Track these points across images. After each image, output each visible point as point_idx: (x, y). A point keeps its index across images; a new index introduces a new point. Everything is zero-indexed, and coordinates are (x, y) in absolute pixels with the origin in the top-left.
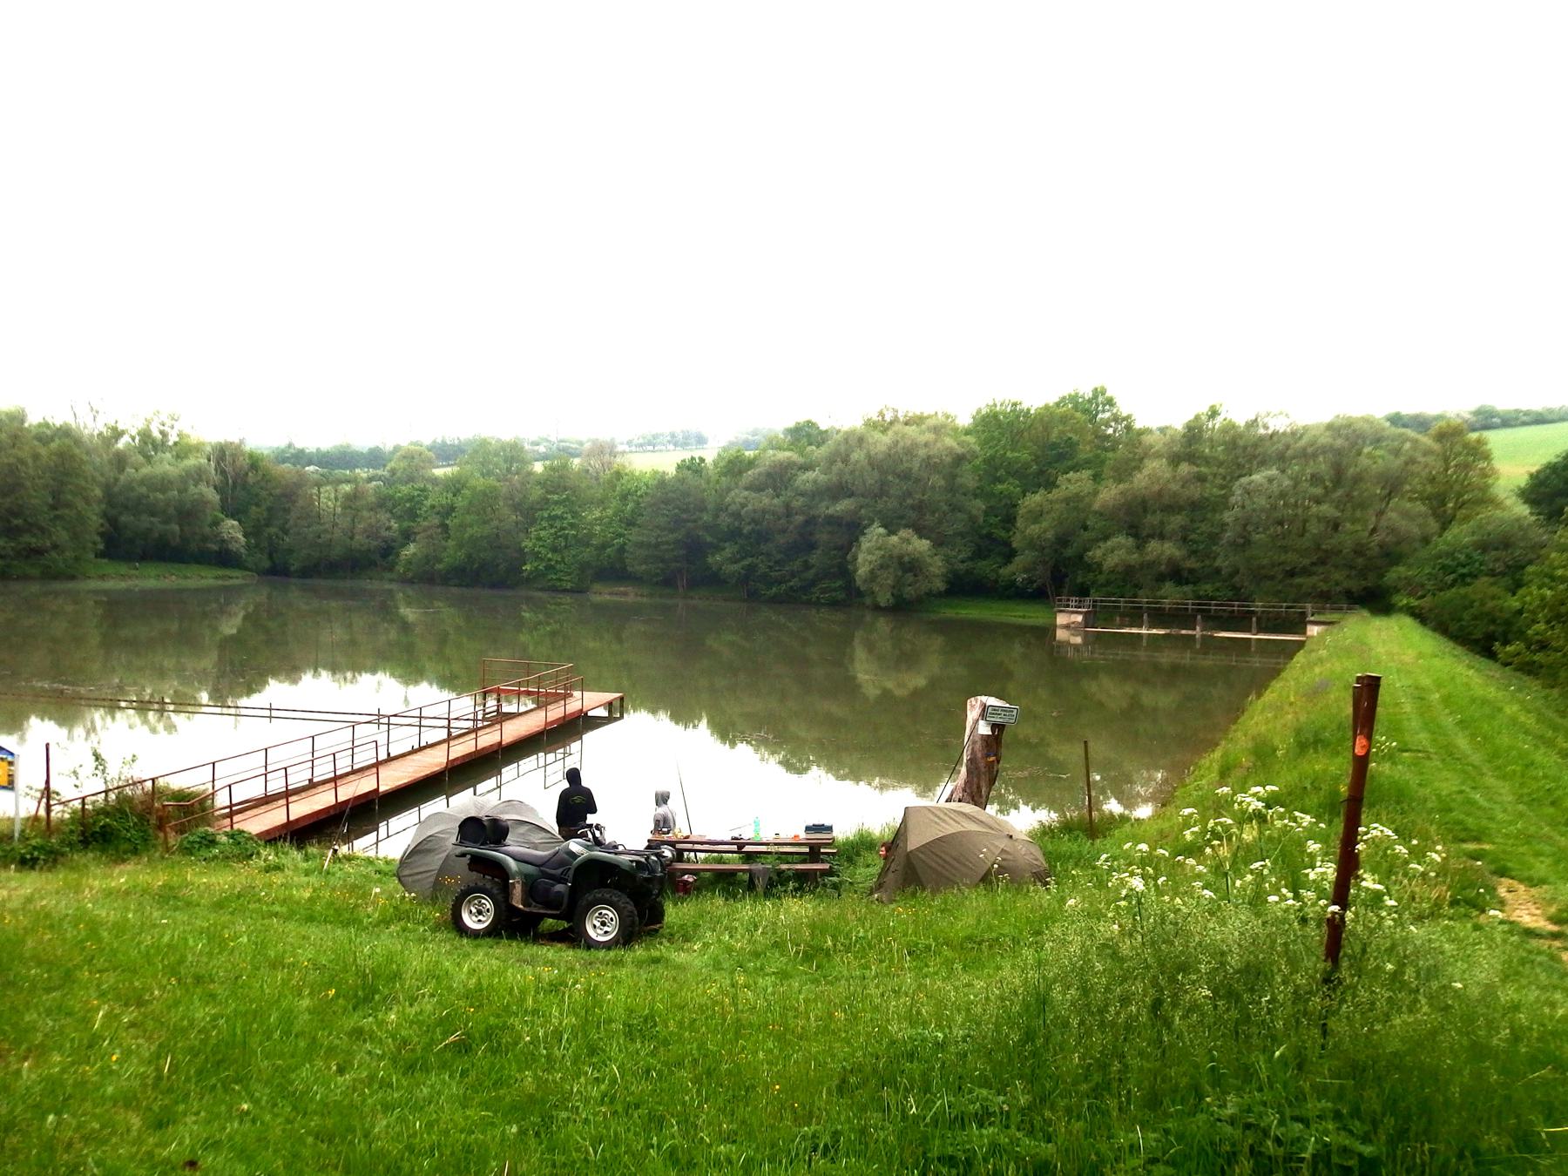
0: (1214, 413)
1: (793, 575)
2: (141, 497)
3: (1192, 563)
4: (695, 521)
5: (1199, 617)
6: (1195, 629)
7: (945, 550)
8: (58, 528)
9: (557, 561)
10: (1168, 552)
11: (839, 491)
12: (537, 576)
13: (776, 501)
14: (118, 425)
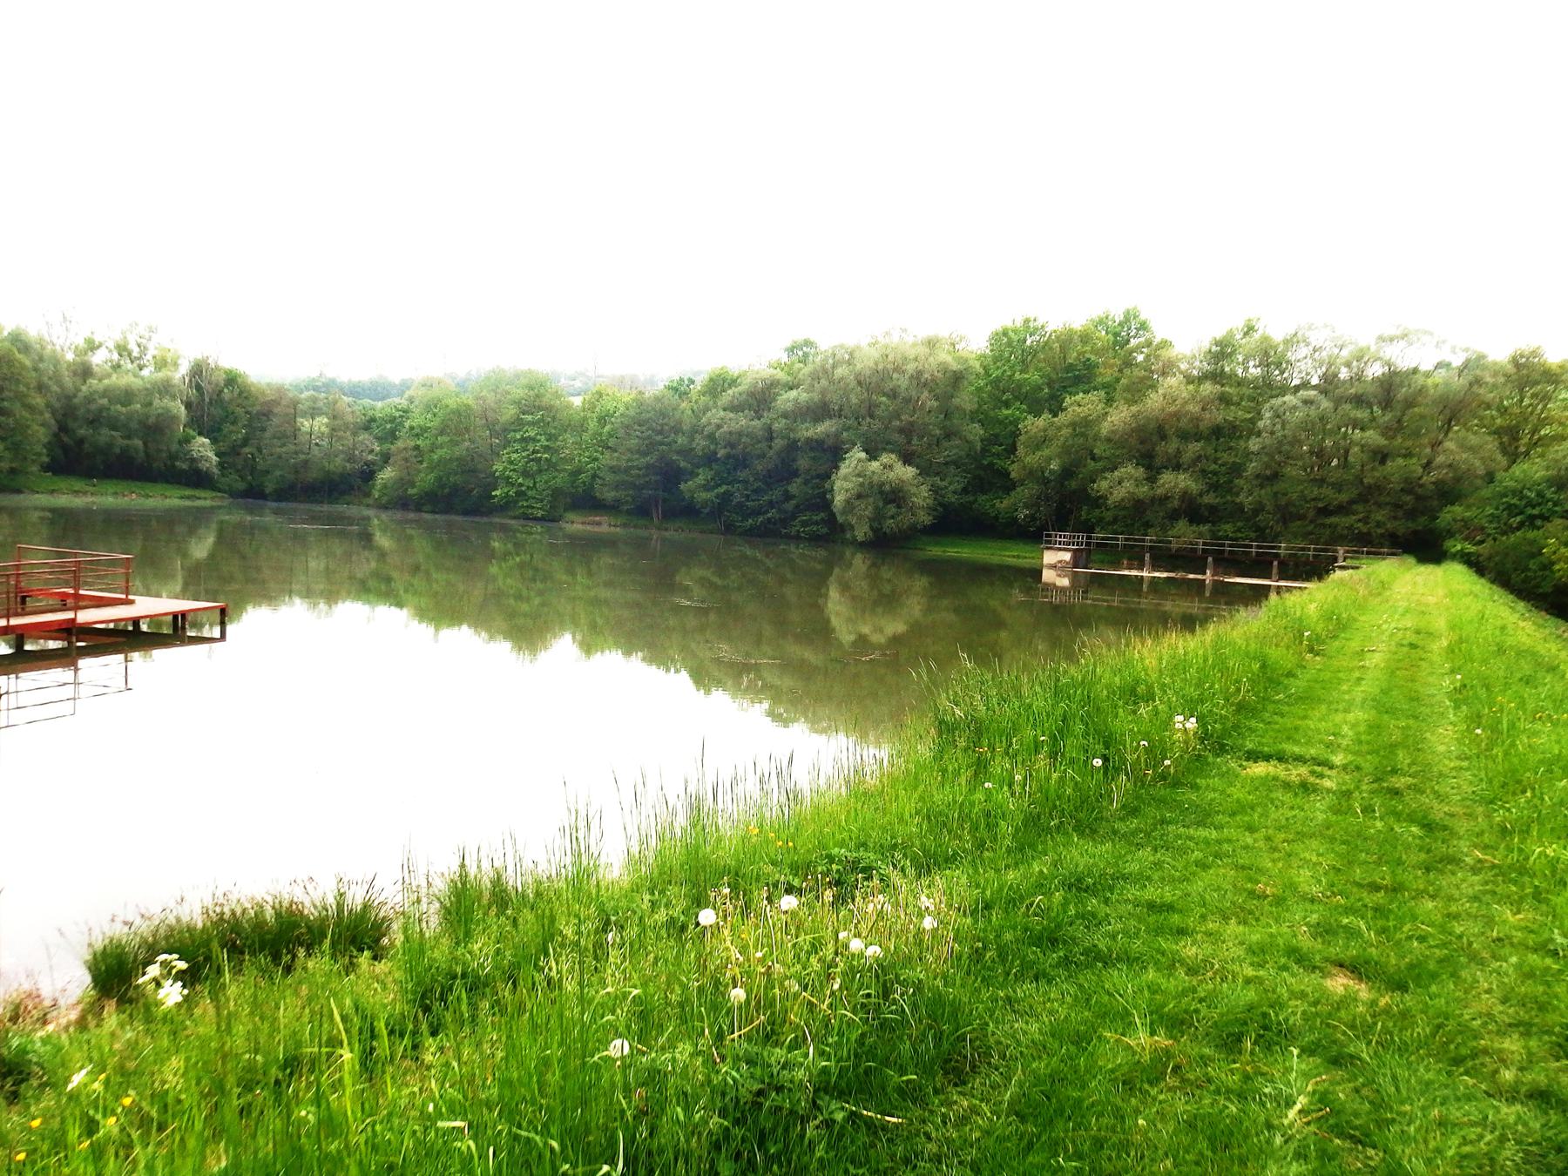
0: (1249, 330)
2: (101, 410)
3: (1209, 499)
4: (669, 444)
5: (1210, 559)
6: (1205, 573)
7: (930, 480)
9: (528, 487)
10: (1182, 485)
11: (820, 411)
13: (755, 423)
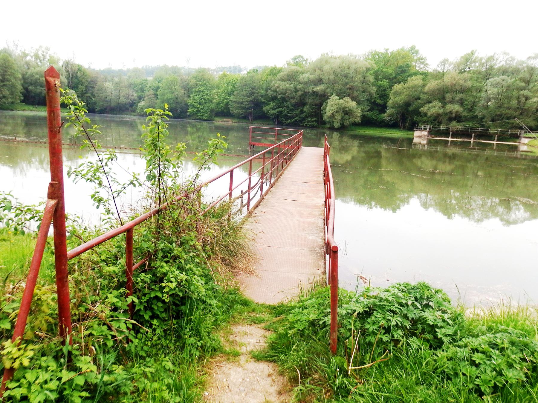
1: (296, 115)
2: (36, 79)
3: (465, 114)
4: (258, 93)
8: (5, 89)
12: (193, 114)
14: (26, 52)
